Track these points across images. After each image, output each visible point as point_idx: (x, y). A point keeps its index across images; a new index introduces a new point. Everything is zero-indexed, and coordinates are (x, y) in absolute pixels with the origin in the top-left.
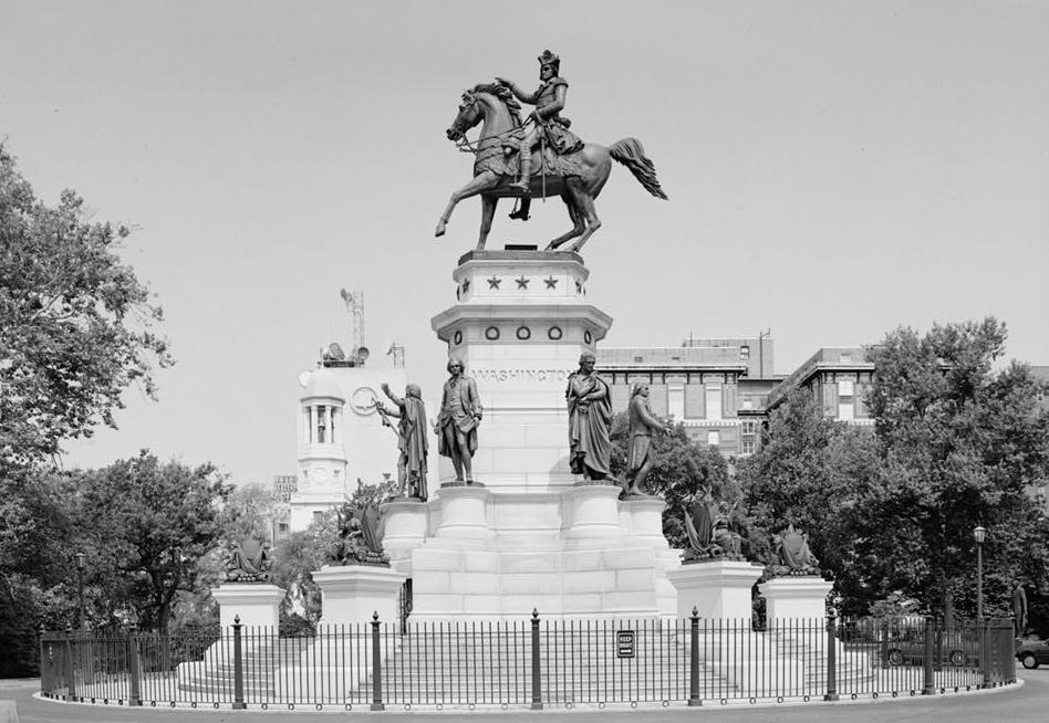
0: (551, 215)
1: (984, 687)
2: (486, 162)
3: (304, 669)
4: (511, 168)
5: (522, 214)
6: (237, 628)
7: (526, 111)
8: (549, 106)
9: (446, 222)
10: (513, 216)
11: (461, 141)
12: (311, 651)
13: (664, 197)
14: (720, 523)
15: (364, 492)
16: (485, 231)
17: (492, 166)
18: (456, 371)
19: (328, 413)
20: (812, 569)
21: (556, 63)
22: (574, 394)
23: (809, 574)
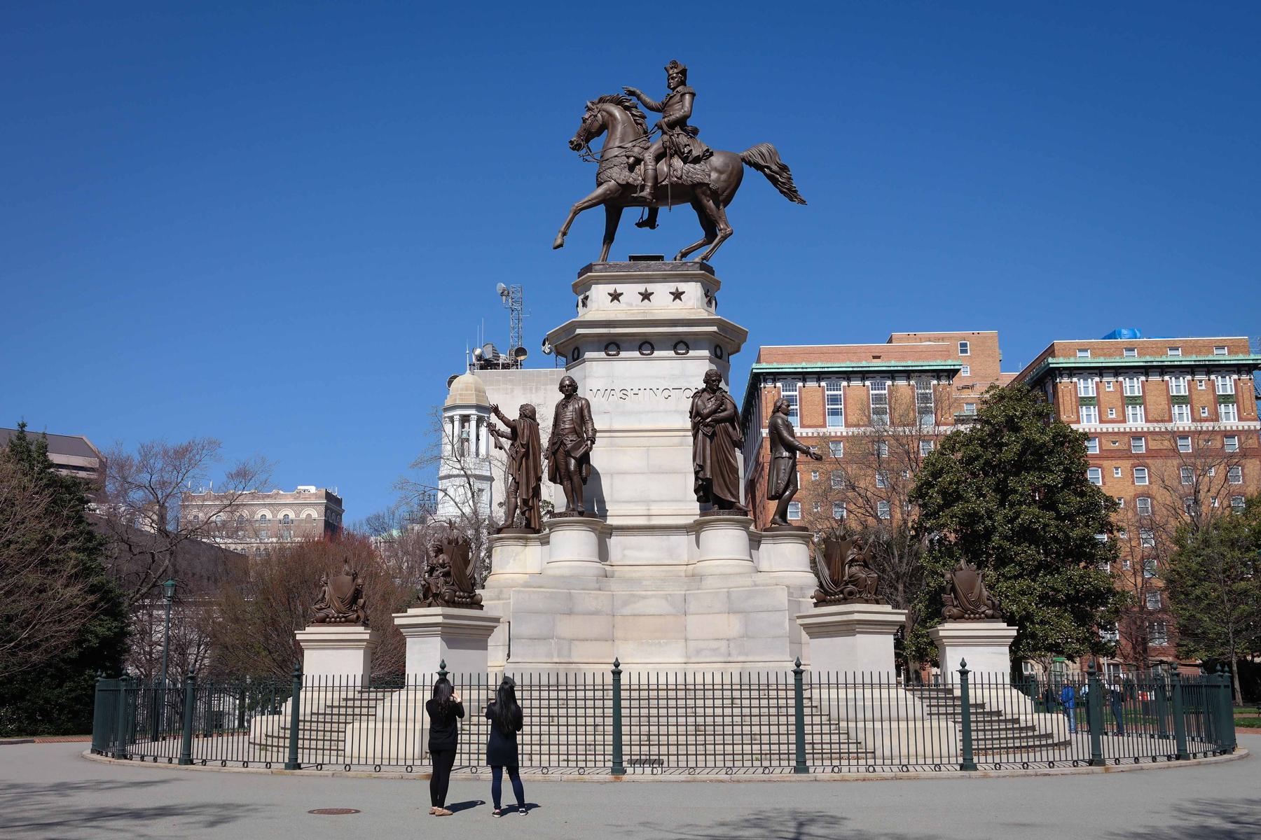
0: (680, 221)
1: (1178, 758)
3: (379, 725)
4: (635, 178)
5: (650, 222)
6: (964, 673)
7: (653, 118)
9: (564, 234)
10: (639, 225)
11: (583, 152)
12: (387, 704)
13: (803, 202)
14: (853, 560)
16: (609, 238)
17: (615, 176)
18: (569, 390)
19: (473, 423)
20: (989, 612)
22: (698, 414)
23: (987, 616)
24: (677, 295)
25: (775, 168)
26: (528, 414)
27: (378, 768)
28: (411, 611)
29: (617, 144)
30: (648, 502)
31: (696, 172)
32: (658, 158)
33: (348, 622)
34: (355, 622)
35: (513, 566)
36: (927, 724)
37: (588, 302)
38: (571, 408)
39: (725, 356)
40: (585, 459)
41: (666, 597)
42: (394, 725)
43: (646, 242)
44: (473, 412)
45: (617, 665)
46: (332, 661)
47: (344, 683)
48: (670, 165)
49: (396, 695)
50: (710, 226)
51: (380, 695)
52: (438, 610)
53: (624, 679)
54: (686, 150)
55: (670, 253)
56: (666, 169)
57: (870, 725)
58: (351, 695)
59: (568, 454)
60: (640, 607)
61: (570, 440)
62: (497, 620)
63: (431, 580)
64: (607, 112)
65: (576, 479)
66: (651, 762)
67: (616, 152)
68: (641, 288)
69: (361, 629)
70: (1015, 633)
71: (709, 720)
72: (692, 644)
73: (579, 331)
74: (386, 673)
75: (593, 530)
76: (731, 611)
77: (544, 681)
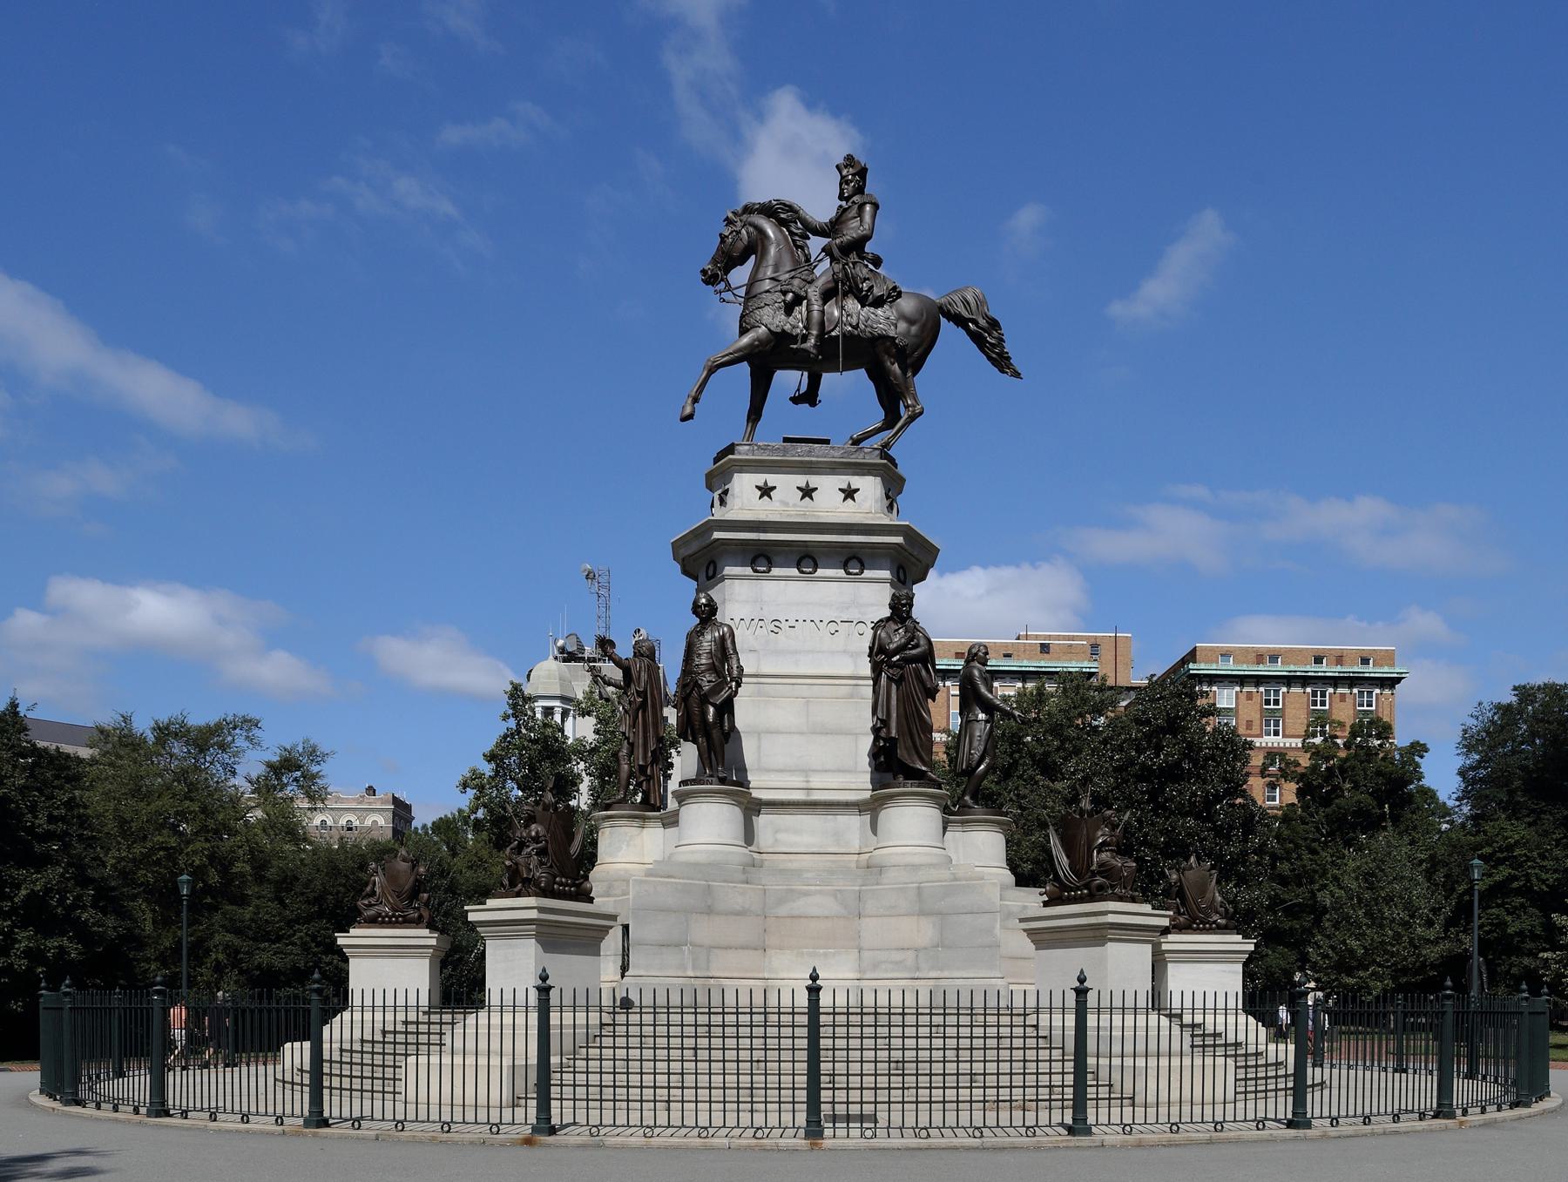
0: (848, 390)
5: (809, 397)
7: (816, 244)
8: (853, 230)
9: (696, 400)
10: (796, 400)
11: (722, 286)
13: (1017, 375)
14: (1104, 844)
16: (755, 414)
17: (766, 320)
18: (706, 614)
21: (862, 173)
24: (849, 493)
25: (982, 322)
26: (647, 653)
27: (447, 1126)
28: (491, 903)
29: (769, 273)
30: (806, 772)
32: (827, 296)
33: (406, 922)
34: (416, 923)
35: (628, 852)
36: (1187, 1061)
37: (729, 499)
38: (708, 637)
39: (909, 581)
40: (727, 708)
41: (834, 894)
42: (470, 1060)
43: (805, 420)
44: (557, 703)
45: (1082, 980)
46: (387, 972)
47: (401, 1001)
48: (842, 308)
49: (471, 1019)
50: (892, 397)
51: (447, 1018)
52: (531, 901)
53: (825, 1000)
54: (865, 286)
56: (836, 313)
57: (1129, 1062)
58: (412, 1017)
59: (705, 700)
60: (800, 906)
61: (707, 681)
62: (613, 918)
63: (520, 859)
65: (715, 733)
66: (862, 1118)
67: (767, 285)
68: (801, 480)
69: (426, 932)
70: (1252, 948)
71: (910, 1055)
72: (866, 954)
73: (717, 535)
74: (460, 985)
75: (739, 804)
76: (922, 913)
77: (675, 1000)
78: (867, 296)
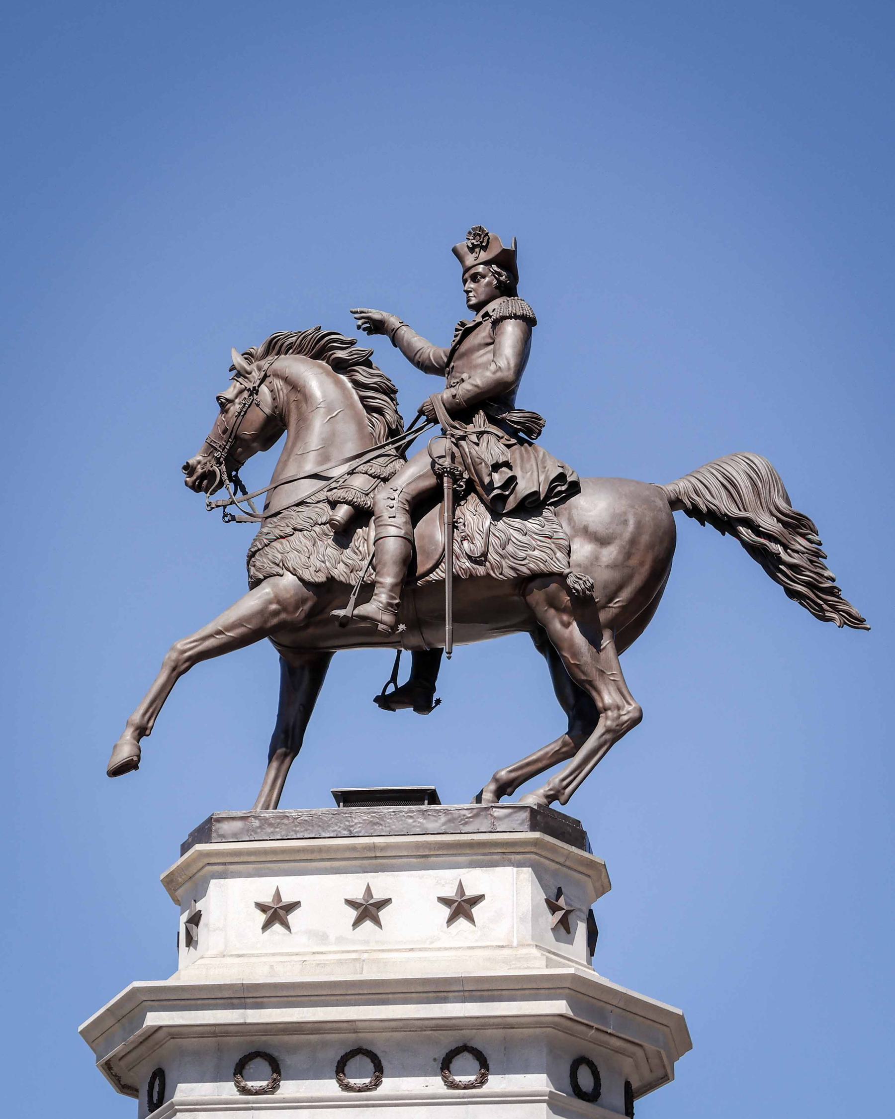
2: (276, 551)
4: (342, 564)
5: (417, 692)
9: (142, 731)
10: (386, 702)
11: (223, 495)
13: (855, 622)
15: (239, 1091)
16: (288, 740)
17: (293, 560)
25: (768, 523)
29: (310, 467)
31: (523, 545)
32: (419, 505)
43: (400, 747)
54: (498, 479)
55: (461, 783)
64: (286, 380)
68: (354, 885)
73: (154, 1019)
78: (502, 499)
